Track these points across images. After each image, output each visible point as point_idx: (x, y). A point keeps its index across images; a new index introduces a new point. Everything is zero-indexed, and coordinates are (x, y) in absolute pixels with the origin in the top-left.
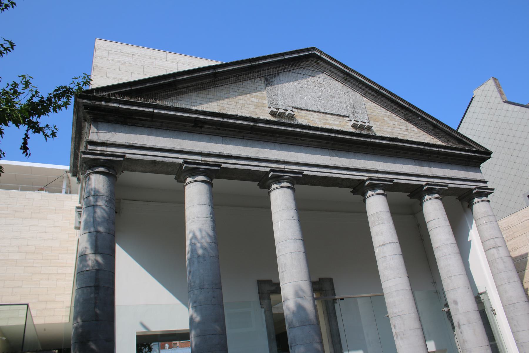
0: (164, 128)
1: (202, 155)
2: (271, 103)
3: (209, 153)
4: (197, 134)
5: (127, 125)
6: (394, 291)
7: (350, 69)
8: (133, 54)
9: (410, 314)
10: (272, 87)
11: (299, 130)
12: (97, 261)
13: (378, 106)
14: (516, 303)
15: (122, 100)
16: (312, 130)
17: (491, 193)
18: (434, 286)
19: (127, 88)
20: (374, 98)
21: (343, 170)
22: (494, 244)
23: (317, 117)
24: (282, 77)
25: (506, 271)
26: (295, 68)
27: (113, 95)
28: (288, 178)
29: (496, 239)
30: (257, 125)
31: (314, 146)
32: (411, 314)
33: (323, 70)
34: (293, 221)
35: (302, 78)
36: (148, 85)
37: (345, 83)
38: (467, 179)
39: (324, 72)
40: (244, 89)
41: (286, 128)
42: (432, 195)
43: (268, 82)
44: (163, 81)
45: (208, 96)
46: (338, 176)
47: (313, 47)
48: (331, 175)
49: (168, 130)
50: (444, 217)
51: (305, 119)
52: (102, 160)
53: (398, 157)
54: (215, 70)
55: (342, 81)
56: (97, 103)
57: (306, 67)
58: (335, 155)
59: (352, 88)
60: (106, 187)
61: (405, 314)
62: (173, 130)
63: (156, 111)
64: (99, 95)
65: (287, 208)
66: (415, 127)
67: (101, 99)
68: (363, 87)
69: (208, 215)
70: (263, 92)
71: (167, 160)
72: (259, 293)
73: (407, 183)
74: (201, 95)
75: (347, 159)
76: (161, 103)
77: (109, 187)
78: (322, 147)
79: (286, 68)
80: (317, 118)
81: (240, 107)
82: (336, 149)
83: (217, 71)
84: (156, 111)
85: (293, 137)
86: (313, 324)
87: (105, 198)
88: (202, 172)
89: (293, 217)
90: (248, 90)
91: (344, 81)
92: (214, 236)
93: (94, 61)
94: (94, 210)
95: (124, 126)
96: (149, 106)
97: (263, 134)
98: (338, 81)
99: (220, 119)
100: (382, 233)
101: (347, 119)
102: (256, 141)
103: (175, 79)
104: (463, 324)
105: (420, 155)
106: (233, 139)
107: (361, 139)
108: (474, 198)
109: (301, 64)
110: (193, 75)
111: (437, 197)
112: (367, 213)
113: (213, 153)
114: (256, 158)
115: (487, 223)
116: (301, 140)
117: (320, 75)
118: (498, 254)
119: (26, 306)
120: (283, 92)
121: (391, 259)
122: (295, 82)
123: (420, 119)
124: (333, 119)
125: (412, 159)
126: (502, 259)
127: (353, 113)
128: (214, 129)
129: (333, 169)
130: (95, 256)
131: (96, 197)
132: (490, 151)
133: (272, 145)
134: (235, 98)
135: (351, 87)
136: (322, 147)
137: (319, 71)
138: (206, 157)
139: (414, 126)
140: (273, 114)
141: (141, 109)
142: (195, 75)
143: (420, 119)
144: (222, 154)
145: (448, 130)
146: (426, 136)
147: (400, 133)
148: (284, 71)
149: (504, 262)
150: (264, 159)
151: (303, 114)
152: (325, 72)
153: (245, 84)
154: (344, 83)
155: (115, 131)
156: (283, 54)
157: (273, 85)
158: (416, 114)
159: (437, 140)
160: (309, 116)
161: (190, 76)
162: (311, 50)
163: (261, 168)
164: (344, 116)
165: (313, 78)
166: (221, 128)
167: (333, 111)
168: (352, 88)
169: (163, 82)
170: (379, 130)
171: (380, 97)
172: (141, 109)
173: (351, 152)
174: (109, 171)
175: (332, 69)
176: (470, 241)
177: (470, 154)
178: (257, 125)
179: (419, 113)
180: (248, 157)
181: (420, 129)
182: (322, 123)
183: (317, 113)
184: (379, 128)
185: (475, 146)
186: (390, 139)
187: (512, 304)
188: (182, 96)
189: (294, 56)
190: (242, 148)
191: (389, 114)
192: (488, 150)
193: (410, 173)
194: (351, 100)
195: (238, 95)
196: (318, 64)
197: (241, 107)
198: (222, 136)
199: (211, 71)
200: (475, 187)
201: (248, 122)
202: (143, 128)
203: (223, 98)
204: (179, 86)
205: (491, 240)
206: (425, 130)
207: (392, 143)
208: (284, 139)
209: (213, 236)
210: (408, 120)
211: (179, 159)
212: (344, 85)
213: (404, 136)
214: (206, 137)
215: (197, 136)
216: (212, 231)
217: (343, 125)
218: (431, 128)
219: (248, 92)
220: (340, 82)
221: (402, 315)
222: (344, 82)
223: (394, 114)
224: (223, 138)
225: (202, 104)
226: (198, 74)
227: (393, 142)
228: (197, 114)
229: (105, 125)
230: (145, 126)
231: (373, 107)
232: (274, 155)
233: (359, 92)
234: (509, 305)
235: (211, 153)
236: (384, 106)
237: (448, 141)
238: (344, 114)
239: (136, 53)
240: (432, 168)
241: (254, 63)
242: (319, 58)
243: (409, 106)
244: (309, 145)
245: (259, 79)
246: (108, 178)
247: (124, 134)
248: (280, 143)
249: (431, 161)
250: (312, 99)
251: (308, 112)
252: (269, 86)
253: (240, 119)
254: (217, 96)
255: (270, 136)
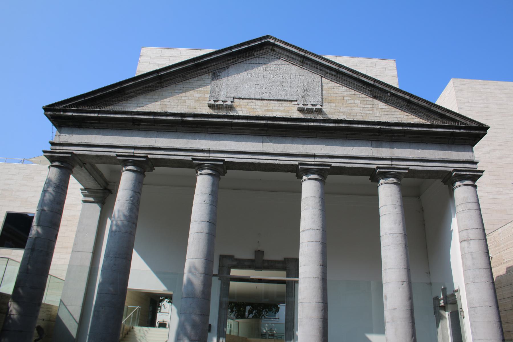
0: (110, 128)
1: (136, 148)
2: (212, 96)
3: (140, 146)
4: (136, 131)
5: (82, 127)
6: (302, 278)
7: (306, 52)
8: (170, 56)
9: (311, 302)
10: (218, 81)
11: (226, 120)
12: (38, 232)
13: (340, 85)
14: (477, 307)
15: (75, 110)
16: (241, 119)
17: (480, 176)
18: (428, 277)
19: (82, 99)
20: (335, 78)
21: (273, 156)
22: (466, 237)
23: (260, 104)
24: (231, 69)
25: (473, 269)
26: (248, 58)
27: (69, 106)
28: (208, 165)
29: (469, 231)
30: (185, 119)
31: (247, 134)
32: (312, 303)
33: (279, 56)
34: (203, 205)
35: (252, 68)
36: (98, 94)
37: (303, 66)
38: (444, 159)
39: (281, 58)
40: (190, 86)
41: (213, 120)
42: (386, 179)
43: (215, 76)
44: (111, 89)
45: (154, 97)
46: (265, 162)
47: (267, 36)
48: (257, 161)
49: (113, 130)
50: (395, 204)
51: (245, 108)
52: (56, 157)
53: (348, 139)
54: (159, 74)
55: (300, 65)
56: (58, 113)
57: (261, 55)
58: (268, 141)
59: (311, 71)
60: (57, 176)
61: (306, 302)
62: (117, 129)
63: (100, 115)
64: (60, 107)
65: (202, 193)
66: (385, 104)
67: (60, 110)
68: (322, 68)
69: (128, 198)
70: (208, 87)
71: (106, 154)
72: (219, 266)
73: (352, 167)
74: (148, 97)
75: (282, 144)
76: (110, 108)
77: (60, 176)
78: (256, 134)
79: (237, 60)
80: (259, 106)
81: (180, 104)
82: (271, 135)
83: (159, 74)
84: (100, 115)
85: (223, 127)
86: (197, 298)
87: (54, 185)
88: (131, 162)
89: (204, 201)
90: (193, 87)
91: (302, 64)
92: (129, 215)
93: (138, 67)
94: (44, 194)
95: (80, 128)
96: (94, 112)
97: (194, 126)
98: (295, 65)
99: (152, 117)
100: (304, 219)
101: (296, 103)
102: (188, 133)
103: (121, 87)
104: (388, 322)
105: (379, 136)
106: (167, 132)
107: (297, 124)
108: (456, 182)
109: (255, 54)
110: (137, 81)
111: (394, 181)
112: (378, 196)
113: (143, 146)
114: (182, 148)
115: (464, 211)
116: (232, 129)
117: (276, 61)
118: (468, 248)
119: (7, 259)
120: (228, 84)
121: (306, 246)
122: (244, 73)
123: (389, 95)
124: (278, 105)
125: (369, 140)
126: (471, 255)
127: (303, 97)
128: (149, 125)
129: (262, 155)
130: (37, 227)
131: (48, 184)
132: (486, 125)
133: (203, 135)
134: (178, 95)
135: (309, 70)
136: (256, 134)
137: (275, 58)
138: (138, 150)
139: (384, 103)
140: (211, 106)
141: (89, 115)
142: (139, 81)
143: (389, 95)
144: (151, 147)
145: (426, 104)
146: (399, 113)
147: (360, 113)
148: (234, 63)
149: (473, 258)
150: (189, 149)
151: (244, 103)
152: (281, 57)
153: (192, 81)
154: (301, 67)
155: (72, 134)
156: (231, 48)
157: (219, 79)
158: (384, 90)
159: (413, 117)
160: (251, 104)
161: (135, 82)
162: (264, 39)
163: (186, 157)
164: (291, 101)
165: (266, 66)
166: (155, 124)
167: (276, 97)
168: (311, 71)
169: (111, 90)
170: (333, 111)
171: (341, 76)
172: (89, 115)
173: (290, 137)
174: (62, 164)
175: (288, 54)
176: (452, 230)
177: (451, 130)
178: (185, 119)
179: (387, 89)
180: (175, 148)
181: (391, 106)
182: (263, 110)
183: (260, 101)
184: (334, 109)
185: (463, 121)
186: (334, 121)
187: (474, 307)
188: (130, 100)
189: (243, 47)
190: (172, 140)
191: (352, 93)
192: (482, 124)
193: (359, 156)
194: (306, 83)
195: (182, 93)
196: (274, 51)
197: (181, 103)
198: (157, 131)
199: (155, 75)
200: (453, 169)
201: (177, 117)
202: (94, 129)
203: (167, 97)
204: (127, 92)
205: (464, 231)
206: (398, 107)
207: (337, 125)
208: (215, 129)
209: (128, 216)
210: (375, 97)
211: (112, 153)
212: (302, 68)
213: (366, 115)
214: (143, 133)
215: (136, 132)
216: (129, 212)
217: (288, 110)
218: (405, 103)
219: (193, 89)
220: (296, 65)
221: (303, 302)
222: (301, 66)
223: (359, 92)
224: (158, 132)
225: (146, 104)
226: (142, 80)
227: (338, 124)
228: (133, 115)
229: (66, 129)
230: (95, 128)
231: (333, 87)
232: (202, 145)
233: (318, 73)
234: (471, 308)
235: (142, 146)
236: (347, 85)
237: (428, 118)
238: (292, 98)
239: (173, 55)
240: (395, 149)
241: (198, 62)
242: (274, 45)
243: (375, 82)
244: (241, 133)
245: (207, 75)
246: (60, 170)
247: (79, 135)
248: (212, 133)
249: (396, 142)
250: (258, 87)
251: (250, 101)
252: (214, 81)
253: (169, 115)
254: (162, 95)
255: (201, 127)
